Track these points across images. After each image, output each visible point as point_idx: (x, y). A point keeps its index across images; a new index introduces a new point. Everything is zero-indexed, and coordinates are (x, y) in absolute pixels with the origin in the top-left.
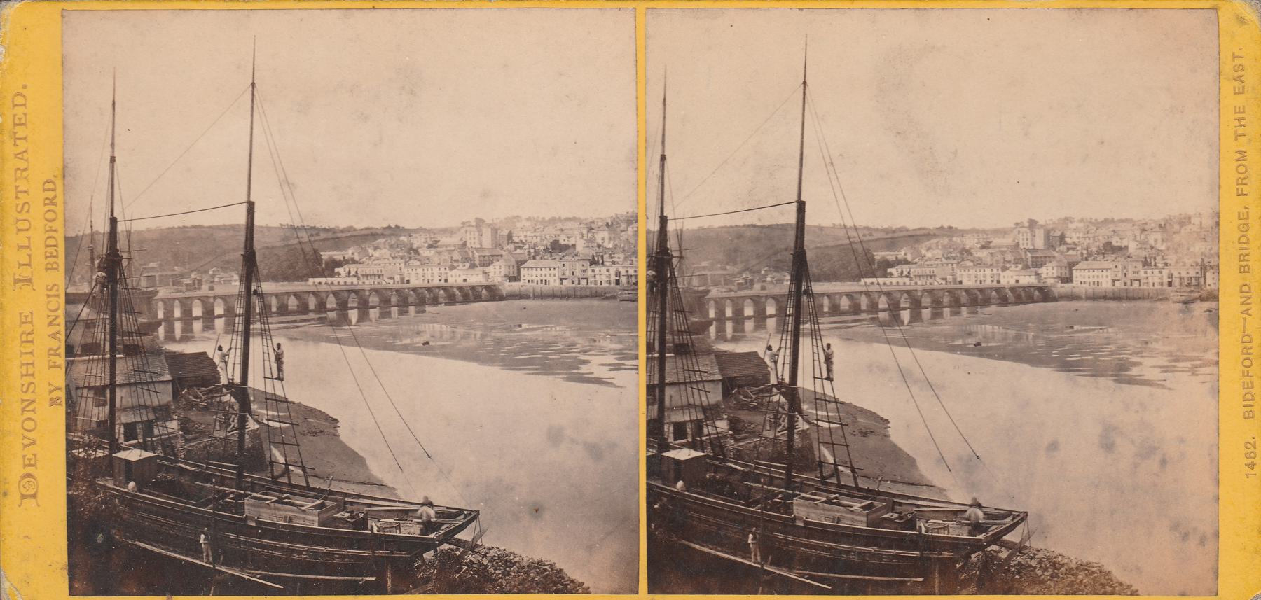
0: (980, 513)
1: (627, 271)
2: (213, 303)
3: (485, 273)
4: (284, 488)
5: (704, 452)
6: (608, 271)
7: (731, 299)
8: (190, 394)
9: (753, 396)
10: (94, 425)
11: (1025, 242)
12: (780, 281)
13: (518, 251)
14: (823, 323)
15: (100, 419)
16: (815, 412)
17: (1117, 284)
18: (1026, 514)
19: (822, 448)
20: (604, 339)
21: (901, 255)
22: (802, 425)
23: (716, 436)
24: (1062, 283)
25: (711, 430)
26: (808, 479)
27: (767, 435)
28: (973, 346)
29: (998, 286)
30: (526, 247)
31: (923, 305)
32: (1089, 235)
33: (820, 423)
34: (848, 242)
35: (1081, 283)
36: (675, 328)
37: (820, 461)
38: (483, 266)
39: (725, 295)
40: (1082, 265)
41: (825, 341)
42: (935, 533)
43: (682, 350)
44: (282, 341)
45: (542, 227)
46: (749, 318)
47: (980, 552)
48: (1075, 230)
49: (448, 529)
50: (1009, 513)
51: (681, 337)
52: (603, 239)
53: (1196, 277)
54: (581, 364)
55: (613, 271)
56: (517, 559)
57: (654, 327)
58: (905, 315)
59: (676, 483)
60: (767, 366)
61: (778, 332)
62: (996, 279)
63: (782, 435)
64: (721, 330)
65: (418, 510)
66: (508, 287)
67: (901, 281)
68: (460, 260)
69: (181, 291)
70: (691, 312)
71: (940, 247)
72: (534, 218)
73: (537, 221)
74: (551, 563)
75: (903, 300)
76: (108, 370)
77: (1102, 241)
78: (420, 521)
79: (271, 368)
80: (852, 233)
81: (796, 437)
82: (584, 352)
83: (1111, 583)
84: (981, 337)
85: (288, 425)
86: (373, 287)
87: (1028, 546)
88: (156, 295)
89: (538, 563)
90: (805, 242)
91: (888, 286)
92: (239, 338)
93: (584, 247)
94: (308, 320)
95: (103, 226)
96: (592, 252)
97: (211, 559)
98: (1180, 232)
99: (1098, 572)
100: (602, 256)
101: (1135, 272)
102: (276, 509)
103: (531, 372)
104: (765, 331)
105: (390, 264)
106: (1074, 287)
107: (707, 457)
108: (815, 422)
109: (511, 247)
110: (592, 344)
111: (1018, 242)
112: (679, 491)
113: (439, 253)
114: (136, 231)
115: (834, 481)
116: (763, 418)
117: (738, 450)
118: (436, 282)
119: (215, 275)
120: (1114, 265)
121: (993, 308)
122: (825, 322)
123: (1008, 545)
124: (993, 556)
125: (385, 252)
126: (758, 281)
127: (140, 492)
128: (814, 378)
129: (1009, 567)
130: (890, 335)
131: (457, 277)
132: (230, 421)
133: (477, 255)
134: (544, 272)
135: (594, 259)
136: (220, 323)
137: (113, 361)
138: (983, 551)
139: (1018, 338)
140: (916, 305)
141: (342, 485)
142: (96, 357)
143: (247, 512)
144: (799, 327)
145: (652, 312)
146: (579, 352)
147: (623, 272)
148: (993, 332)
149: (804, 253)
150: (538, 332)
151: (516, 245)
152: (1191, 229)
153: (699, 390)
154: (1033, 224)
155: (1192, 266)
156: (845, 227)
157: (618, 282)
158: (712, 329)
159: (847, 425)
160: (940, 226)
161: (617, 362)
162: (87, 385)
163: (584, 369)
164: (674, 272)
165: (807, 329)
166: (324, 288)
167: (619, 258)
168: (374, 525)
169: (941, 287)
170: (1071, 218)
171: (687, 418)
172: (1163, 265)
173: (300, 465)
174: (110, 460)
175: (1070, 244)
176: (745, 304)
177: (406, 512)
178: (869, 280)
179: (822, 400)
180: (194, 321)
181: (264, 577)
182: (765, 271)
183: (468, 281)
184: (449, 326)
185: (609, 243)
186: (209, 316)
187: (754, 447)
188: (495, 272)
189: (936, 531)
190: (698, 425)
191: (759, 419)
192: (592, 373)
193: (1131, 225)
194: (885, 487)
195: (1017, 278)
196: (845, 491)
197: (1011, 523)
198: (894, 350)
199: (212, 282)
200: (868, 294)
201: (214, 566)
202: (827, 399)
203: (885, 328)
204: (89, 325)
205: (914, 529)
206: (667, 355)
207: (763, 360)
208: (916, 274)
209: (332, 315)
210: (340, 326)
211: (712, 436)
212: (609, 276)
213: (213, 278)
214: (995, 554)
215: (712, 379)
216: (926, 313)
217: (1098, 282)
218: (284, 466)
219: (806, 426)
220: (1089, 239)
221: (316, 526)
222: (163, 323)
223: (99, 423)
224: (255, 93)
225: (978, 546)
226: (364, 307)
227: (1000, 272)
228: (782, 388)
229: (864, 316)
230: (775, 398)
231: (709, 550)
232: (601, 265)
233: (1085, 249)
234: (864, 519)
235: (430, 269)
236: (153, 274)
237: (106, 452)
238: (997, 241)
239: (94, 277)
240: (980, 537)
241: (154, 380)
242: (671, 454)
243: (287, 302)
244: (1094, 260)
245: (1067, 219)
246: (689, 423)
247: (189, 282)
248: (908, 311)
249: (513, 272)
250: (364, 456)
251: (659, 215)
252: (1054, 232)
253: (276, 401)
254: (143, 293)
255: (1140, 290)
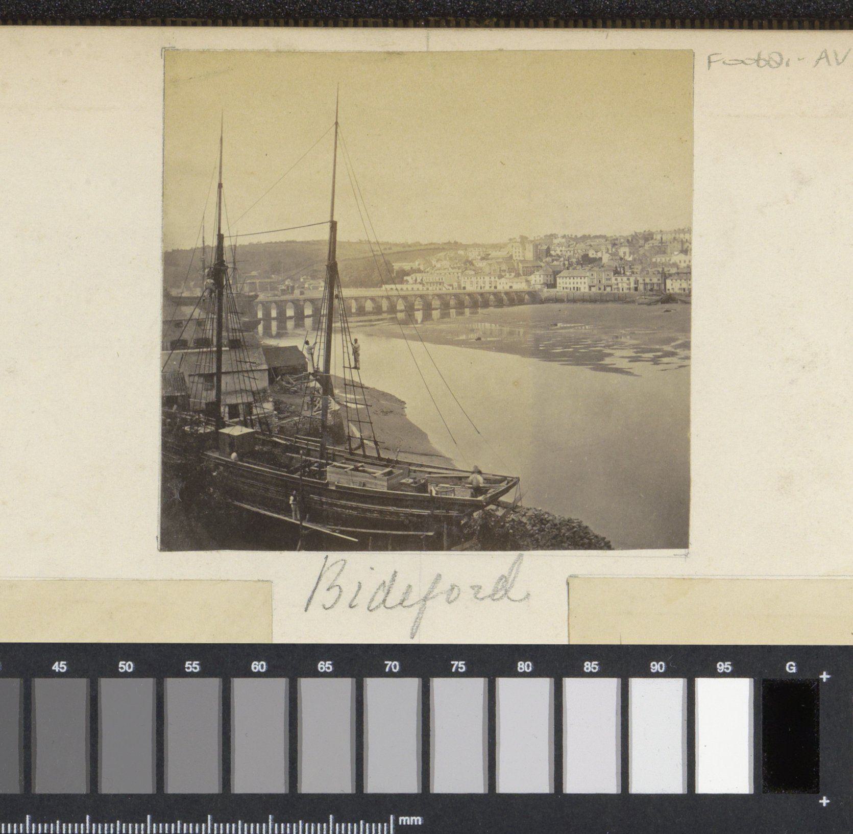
0: (480, 478)
1: (644, 280)
2: (303, 306)
3: (527, 281)
4: (361, 459)
5: (253, 429)
6: (628, 279)
7: (275, 302)
8: (282, 380)
9: (294, 383)
10: (204, 406)
11: (517, 254)
12: (316, 288)
13: (555, 263)
14: (351, 322)
15: (208, 401)
16: (344, 395)
17: (593, 289)
18: (518, 479)
19: (350, 424)
20: (625, 335)
21: (415, 265)
22: (334, 406)
23: (264, 415)
24: (547, 288)
25: (259, 411)
26: (339, 451)
27: (305, 415)
28: (474, 340)
29: (496, 290)
30: (562, 259)
31: (433, 307)
32: (570, 249)
33: (349, 405)
34: (371, 254)
35: (563, 288)
36: (230, 327)
37: (349, 436)
38: (527, 275)
39: (271, 299)
40: (565, 273)
41: (353, 337)
42: (443, 495)
43: (235, 344)
44: (361, 338)
45: (575, 243)
46: (291, 318)
47: (481, 511)
48: (559, 245)
49: (493, 493)
50: (504, 478)
51: (234, 334)
52: (625, 253)
53: (657, 284)
54: (606, 357)
55: (632, 279)
56: (551, 518)
57: (213, 325)
58: (419, 315)
59: (230, 454)
60: (305, 358)
61: (314, 329)
62: (493, 285)
63: (317, 414)
64: (267, 328)
65: (468, 477)
66: (546, 293)
67: (415, 287)
68: (507, 270)
69: (277, 296)
70: (242, 313)
71: (448, 259)
72: (568, 236)
73: (571, 238)
74: (579, 521)
75: (417, 303)
76: (215, 360)
77: (581, 253)
78: (471, 486)
79: (349, 360)
80: (376, 248)
81: (329, 416)
82: (608, 346)
83: (588, 536)
84: (481, 333)
85: (363, 406)
86: (435, 292)
87: (520, 505)
88: (256, 299)
89: (568, 522)
90: (336, 255)
91: (404, 291)
92: (323, 334)
93: (609, 260)
94: (382, 320)
95: (212, 242)
96: (616, 264)
97: (298, 517)
98: (644, 246)
99: (578, 527)
100: (624, 268)
101: (607, 279)
102: (352, 476)
103: (567, 363)
104: (304, 328)
105: (449, 274)
106: (558, 292)
107: (256, 432)
108: (345, 403)
109: (549, 259)
110: (615, 340)
111: (512, 255)
112: (233, 461)
113: (490, 265)
114: (240, 245)
115: (360, 452)
116: (302, 400)
117: (282, 427)
118: (487, 288)
119: (305, 282)
120: (591, 274)
121: (491, 309)
122: (353, 321)
123: (505, 506)
124: (491, 514)
125: (446, 263)
126: (298, 287)
127: (241, 461)
128: (344, 367)
129: (504, 523)
130: (407, 331)
131: (503, 285)
132: (316, 403)
133: (521, 265)
134: (576, 280)
135: (617, 269)
136: (308, 322)
137: (219, 352)
138: (483, 510)
139: (511, 333)
140: (428, 309)
141: (407, 455)
142: (205, 350)
143: (328, 477)
144: (332, 325)
145: (210, 314)
146: (604, 347)
147: (641, 281)
148: (491, 329)
149: (335, 264)
150: (572, 330)
151: (553, 258)
152: (653, 244)
153: (249, 378)
154: (523, 239)
155: (654, 274)
156: (369, 242)
157: (636, 289)
158: (260, 328)
159: (371, 406)
160: (448, 241)
161: (634, 355)
162: (197, 372)
163: (607, 361)
164: (229, 280)
165: (339, 327)
166: (394, 293)
167: (637, 269)
168: (433, 490)
169: (448, 292)
170: (555, 234)
171: (240, 401)
172: (630, 273)
173: (373, 439)
174: (216, 435)
175: (554, 256)
176: (287, 306)
177: (460, 478)
178: (388, 287)
179: (351, 385)
180: (288, 320)
181: (342, 532)
182: (304, 279)
183: (514, 288)
184: (497, 325)
185: (630, 256)
186: (300, 317)
187: (294, 424)
188: (535, 281)
189: (444, 493)
190: (249, 406)
191: (298, 401)
192: (615, 364)
193: (605, 240)
194: (402, 457)
195: (511, 284)
196: (369, 461)
197: (506, 486)
198: (426, 346)
199: (303, 288)
200: (388, 298)
201: (301, 523)
202: (355, 384)
203: (402, 326)
204: (200, 323)
205: (426, 492)
206: (223, 349)
207: (301, 353)
208: (428, 281)
209: (401, 316)
210: (407, 325)
211: (260, 416)
212: (629, 284)
213: (304, 285)
214: (493, 512)
215: (260, 368)
216: (436, 314)
217: (577, 288)
218: (359, 440)
219: (337, 407)
220: (570, 252)
221: (385, 490)
222: (262, 322)
223: (207, 404)
224: (339, 131)
225: (478, 506)
226: (428, 309)
227: (497, 279)
228: (317, 375)
229: (385, 316)
230: (312, 384)
231: (258, 510)
232: (623, 275)
233: (566, 260)
234: (385, 484)
235: (469, 278)
236: (254, 281)
237: (213, 428)
238: (494, 254)
239: (205, 283)
240: (480, 498)
241: (253, 368)
242: (226, 431)
243: (365, 305)
244: (574, 269)
245: (552, 235)
246: (242, 405)
247: (284, 288)
248: (421, 312)
249: (551, 280)
250: (427, 432)
251: (217, 233)
252: (542, 246)
253: (354, 386)
254: (246, 297)
255: (611, 293)
